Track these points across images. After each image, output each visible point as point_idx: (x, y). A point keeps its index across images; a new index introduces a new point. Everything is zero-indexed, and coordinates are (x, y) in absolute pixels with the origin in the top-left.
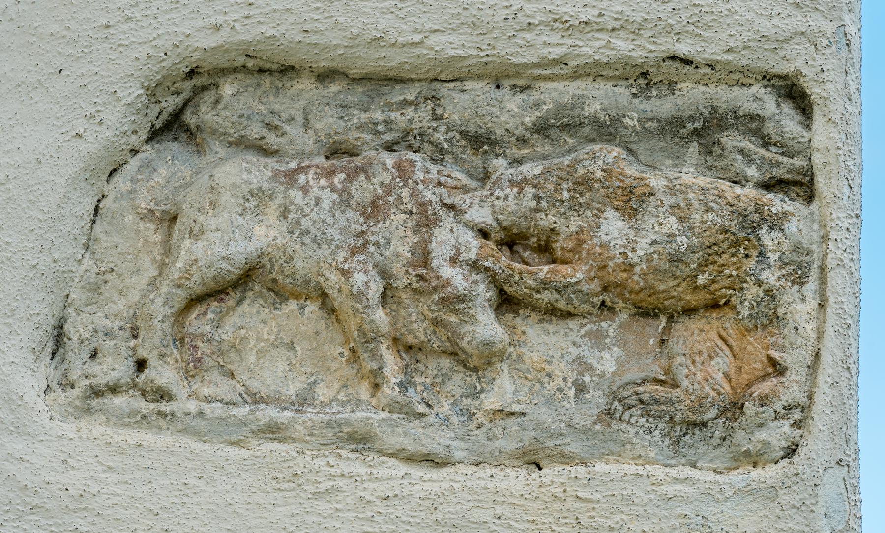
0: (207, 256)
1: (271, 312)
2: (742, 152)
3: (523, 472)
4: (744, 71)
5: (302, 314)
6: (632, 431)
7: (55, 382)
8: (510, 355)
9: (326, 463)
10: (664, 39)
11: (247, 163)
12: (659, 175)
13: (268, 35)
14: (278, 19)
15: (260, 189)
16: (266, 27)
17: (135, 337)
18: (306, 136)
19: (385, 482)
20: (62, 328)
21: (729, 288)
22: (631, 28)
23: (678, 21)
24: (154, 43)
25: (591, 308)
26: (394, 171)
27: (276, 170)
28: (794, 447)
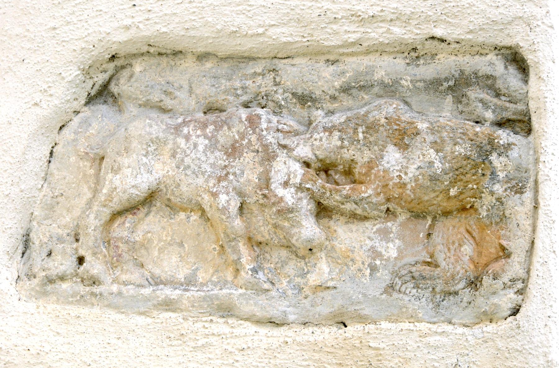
0: (123, 185)
1: (168, 221)
2: (481, 101)
3: (334, 329)
4: (483, 45)
5: (189, 222)
6: (406, 298)
7: (23, 274)
8: (326, 247)
9: (202, 326)
10: (426, 26)
11: (150, 119)
12: (424, 120)
13: (162, 32)
14: (169, 20)
15: (157, 138)
16: (160, 26)
17: (77, 240)
18: (191, 98)
19: (242, 338)
20: (29, 235)
21: (472, 197)
22: (404, 19)
23: (435, 13)
24: (86, 39)
25: (380, 213)
26: (246, 123)
27: (169, 124)
28: (518, 307)
